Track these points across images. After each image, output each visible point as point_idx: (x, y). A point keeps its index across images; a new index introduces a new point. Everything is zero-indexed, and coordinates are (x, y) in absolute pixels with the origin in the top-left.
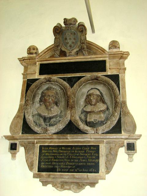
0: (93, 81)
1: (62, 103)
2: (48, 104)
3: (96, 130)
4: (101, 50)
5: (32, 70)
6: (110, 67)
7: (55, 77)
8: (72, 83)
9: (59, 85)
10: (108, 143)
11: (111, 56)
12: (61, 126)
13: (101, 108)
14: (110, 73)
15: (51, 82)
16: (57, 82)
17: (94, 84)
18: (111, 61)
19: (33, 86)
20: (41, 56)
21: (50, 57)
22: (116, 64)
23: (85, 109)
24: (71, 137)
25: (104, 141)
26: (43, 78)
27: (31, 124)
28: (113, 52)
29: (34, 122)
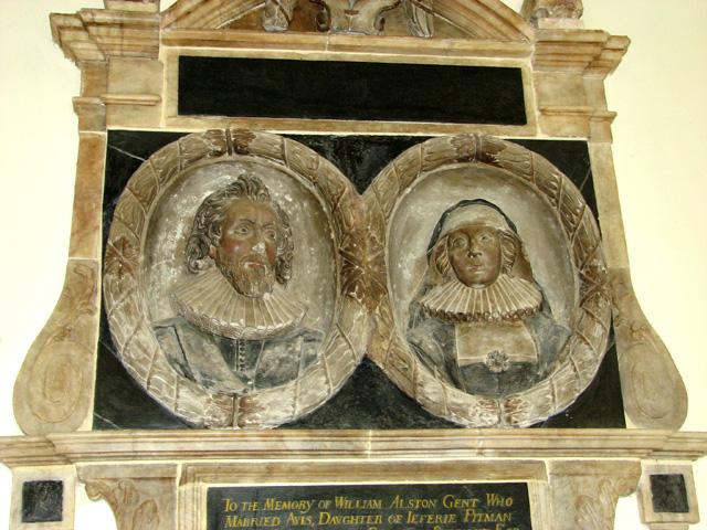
0: (464, 165)
1: (309, 265)
2: (246, 266)
3: (506, 406)
4: (498, 16)
5: (137, 86)
6: (544, 105)
7: (269, 132)
8: (362, 170)
9: (288, 170)
10: (562, 471)
11: (550, 49)
12: (322, 386)
13: (225, 314)
14: (544, 132)
15: (247, 153)
16: (283, 158)
17: (469, 182)
18: (545, 76)
19: (150, 168)
20: (189, 13)
21: (233, 26)
22: (571, 91)
23: (430, 302)
24: (380, 445)
25: (542, 463)
26: (205, 130)
27: (152, 373)
28: (560, 31)
29: (172, 361)
